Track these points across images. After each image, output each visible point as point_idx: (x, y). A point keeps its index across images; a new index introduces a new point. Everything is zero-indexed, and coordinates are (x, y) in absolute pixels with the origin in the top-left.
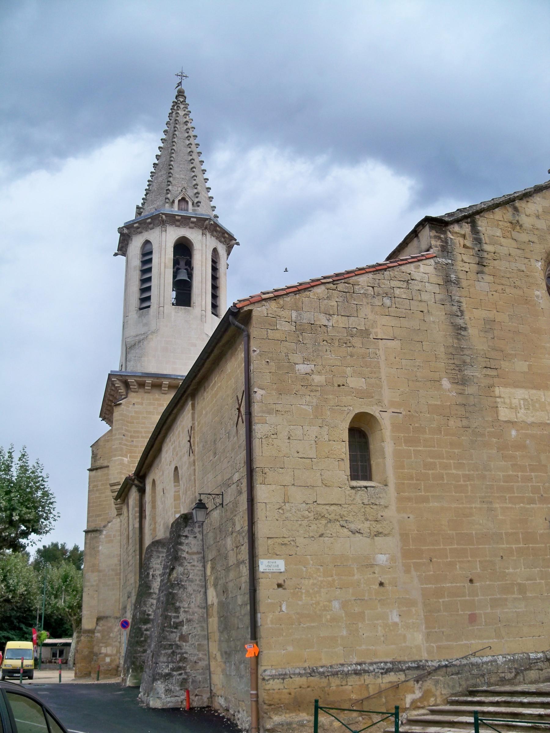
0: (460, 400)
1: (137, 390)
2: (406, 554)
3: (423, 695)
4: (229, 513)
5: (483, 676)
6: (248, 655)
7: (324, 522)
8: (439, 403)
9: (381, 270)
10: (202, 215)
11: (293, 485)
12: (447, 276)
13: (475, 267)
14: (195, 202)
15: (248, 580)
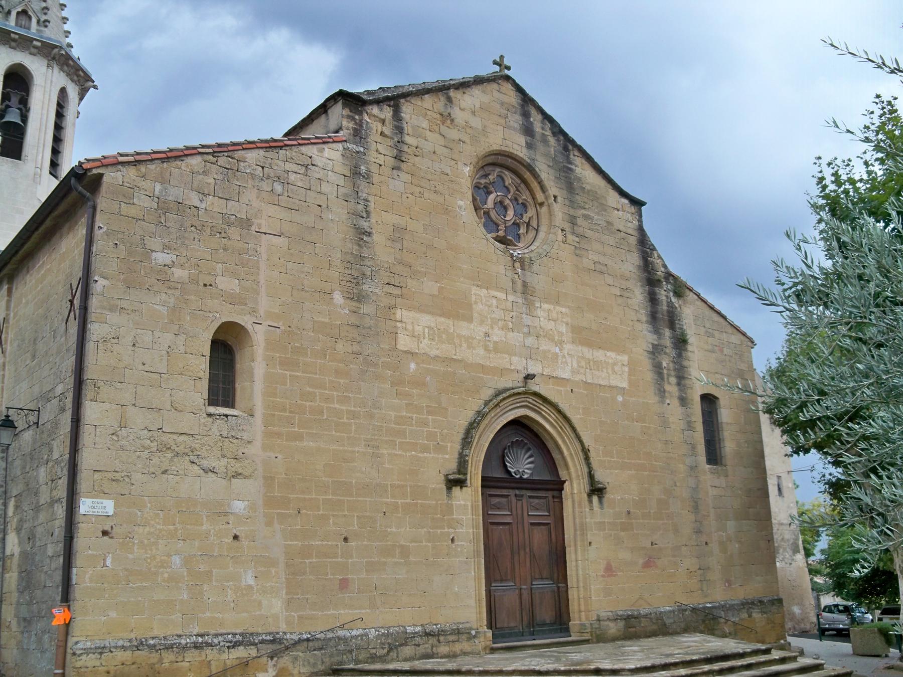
0: (353, 319)
2: (270, 502)
3: (277, 674)
4: (45, 436)
5: (351, 652)
6: (55, 623)
7: (169, 455)
8: (327, 320)
9: (275, 147)
10: (50, 39)
11: (134, 405)
12: (356, 166)
13: (391, 161)
14: (42, 20)
15: (63, 525)
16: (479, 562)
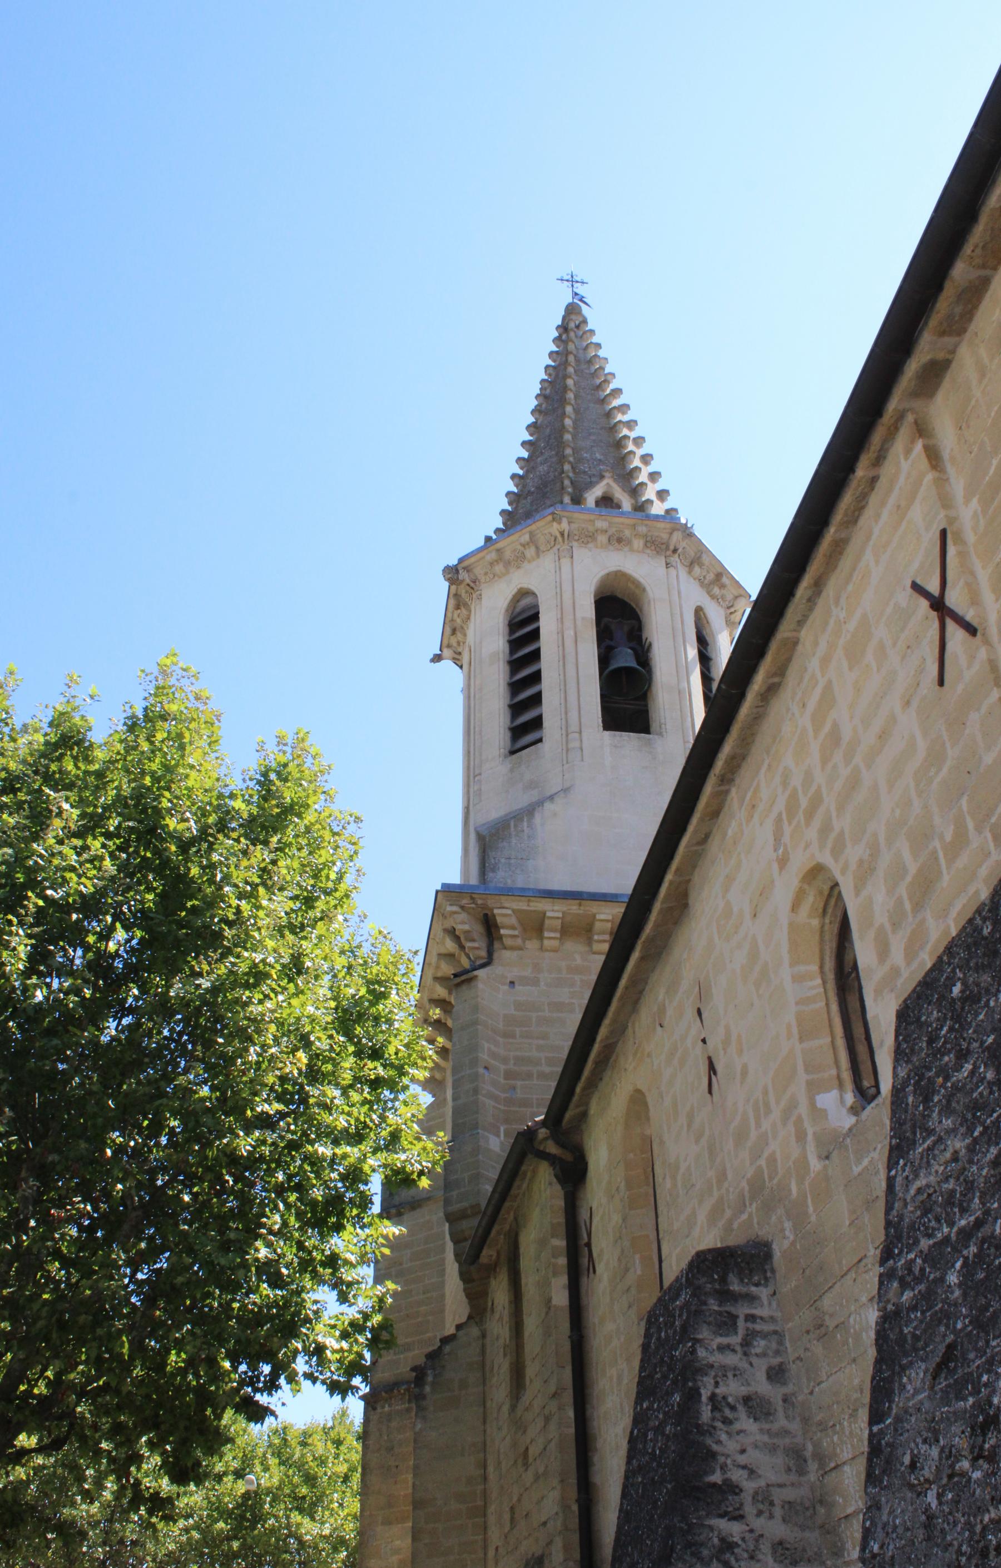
1: (519, 941)
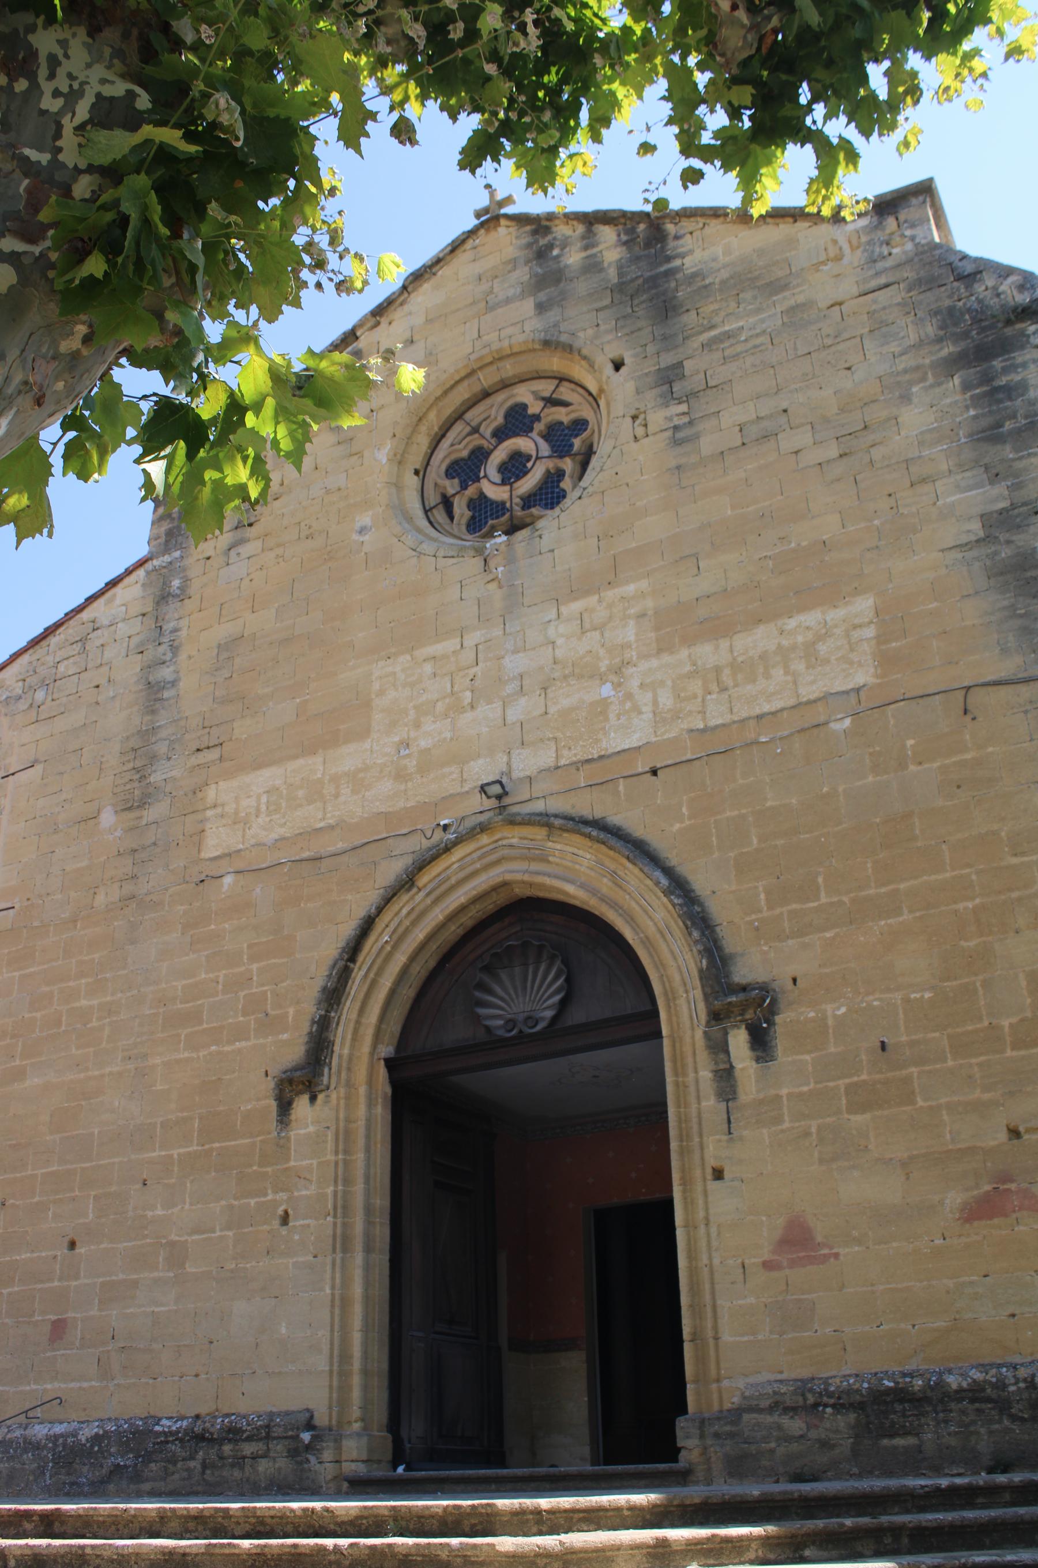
16: (691, 1257)
